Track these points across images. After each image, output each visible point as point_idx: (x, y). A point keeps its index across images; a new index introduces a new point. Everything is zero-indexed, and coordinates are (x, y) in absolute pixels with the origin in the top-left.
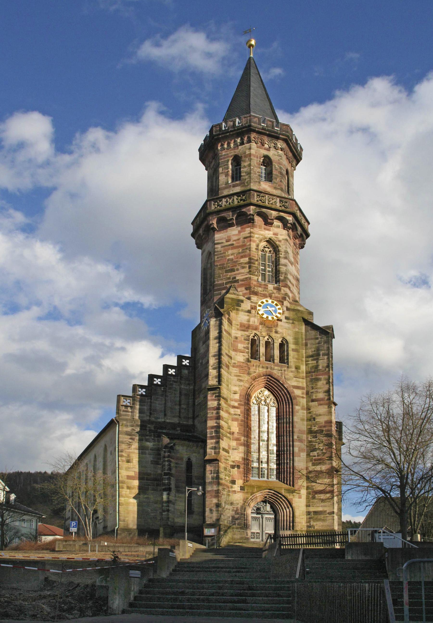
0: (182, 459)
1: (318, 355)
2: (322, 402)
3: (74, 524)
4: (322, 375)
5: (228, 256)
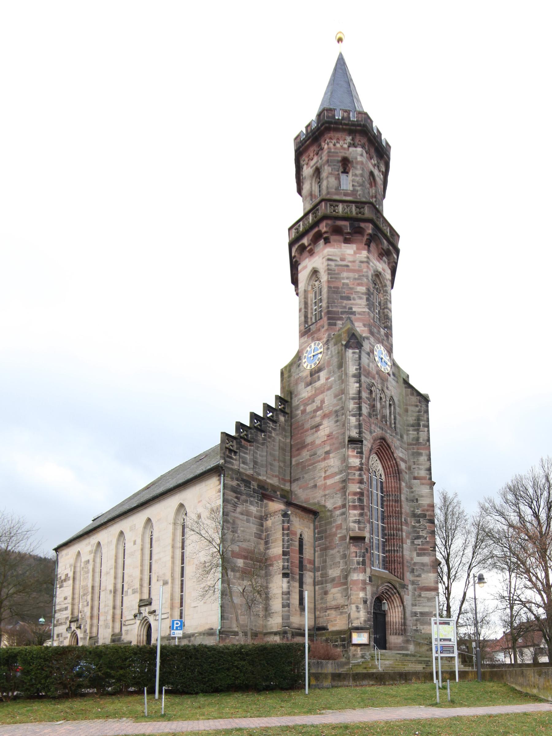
0: (295, 534)
1: (419, 425)
2: (423, 481)
3: (177, 624)
4: (423, 449)
5: (343, 278)
